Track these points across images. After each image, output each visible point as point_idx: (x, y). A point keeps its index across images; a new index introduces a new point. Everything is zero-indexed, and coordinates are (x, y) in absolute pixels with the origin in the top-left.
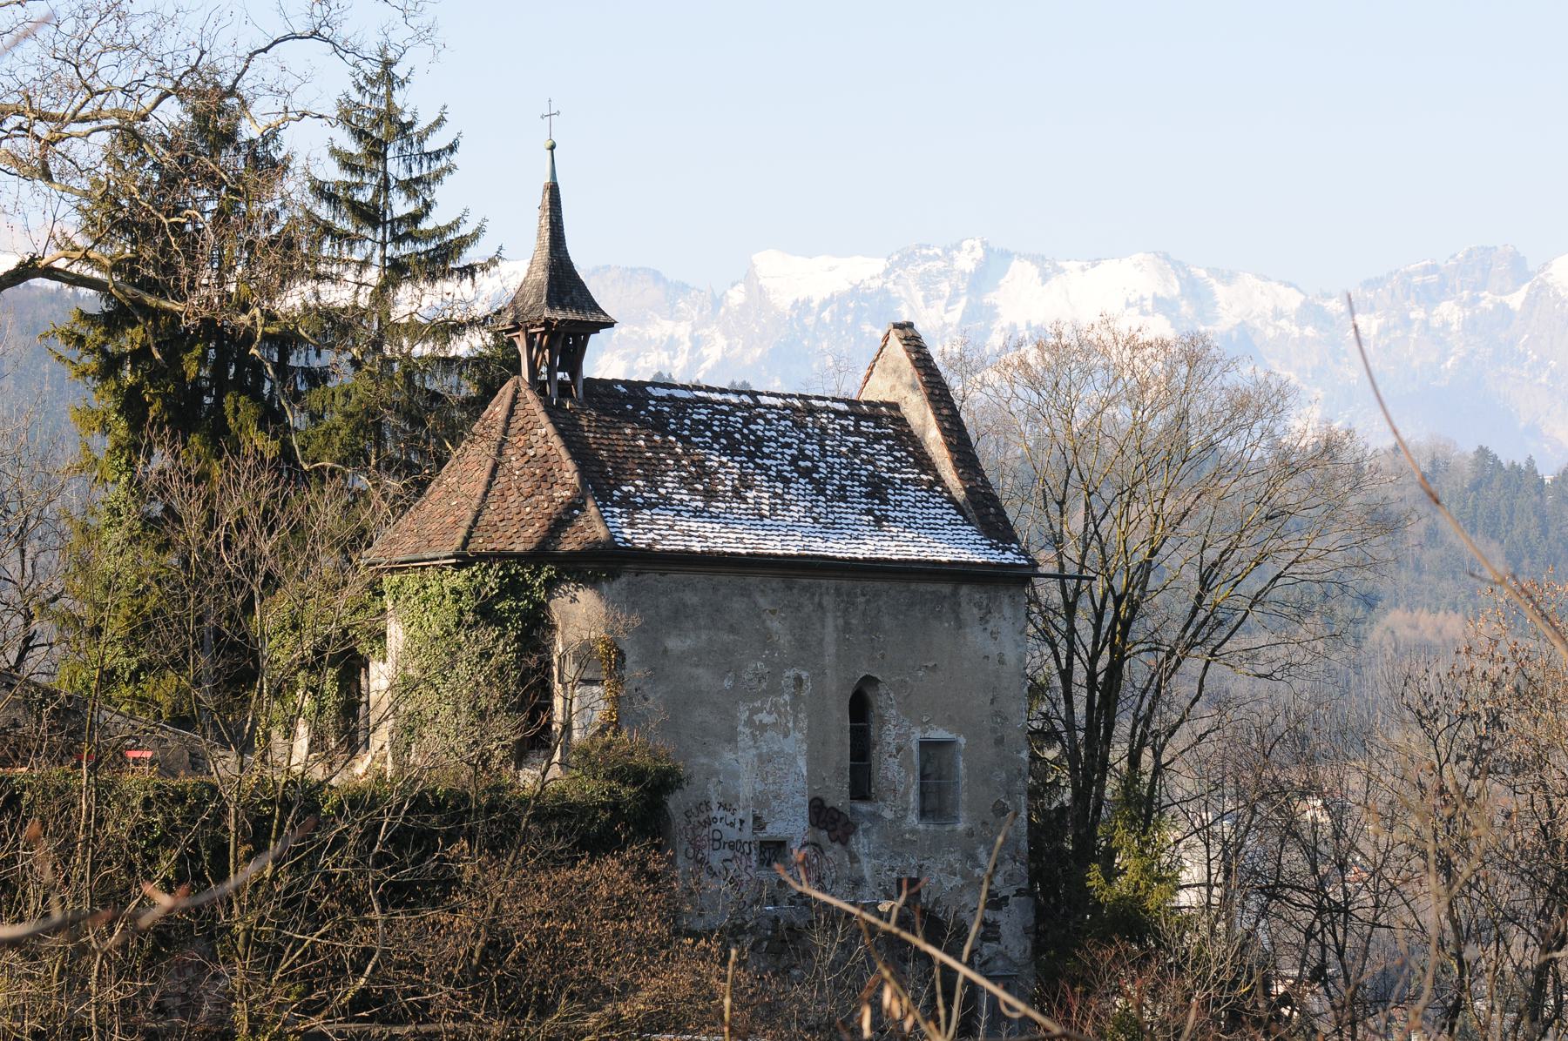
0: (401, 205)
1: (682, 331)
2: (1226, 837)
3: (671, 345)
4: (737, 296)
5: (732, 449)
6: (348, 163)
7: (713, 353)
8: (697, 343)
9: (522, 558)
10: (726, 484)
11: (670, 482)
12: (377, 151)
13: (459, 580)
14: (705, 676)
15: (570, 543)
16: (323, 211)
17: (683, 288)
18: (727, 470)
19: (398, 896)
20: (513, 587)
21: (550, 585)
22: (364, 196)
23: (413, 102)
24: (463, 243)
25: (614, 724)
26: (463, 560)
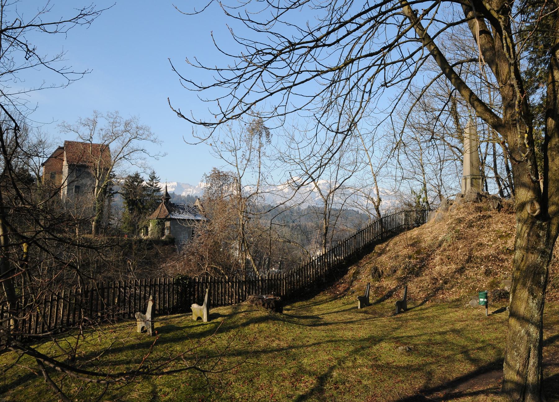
0: (155, 185)
1: (191, 190)
2: (438, 184)
3: (190, 191)
4: (197, 187)
5: (182, 209)
6: (150, 181)
7: (194, 192)
8: (193, 191)
9: (162, 219)
10: (181, 212)
11: (176, 212)
12: (152, 180)
13: (156, 221)
14: (179, 229)
15: (168, 218)
16: (147, 185)
17: (191, 186)
18: (181, 211)
19: (148, 249)
20: (161, 221)
21: (165, 221)
22: (151, 184)
23: (156, 175)
24: (160, 189)
25: (170, 234)
26: (157, 219)
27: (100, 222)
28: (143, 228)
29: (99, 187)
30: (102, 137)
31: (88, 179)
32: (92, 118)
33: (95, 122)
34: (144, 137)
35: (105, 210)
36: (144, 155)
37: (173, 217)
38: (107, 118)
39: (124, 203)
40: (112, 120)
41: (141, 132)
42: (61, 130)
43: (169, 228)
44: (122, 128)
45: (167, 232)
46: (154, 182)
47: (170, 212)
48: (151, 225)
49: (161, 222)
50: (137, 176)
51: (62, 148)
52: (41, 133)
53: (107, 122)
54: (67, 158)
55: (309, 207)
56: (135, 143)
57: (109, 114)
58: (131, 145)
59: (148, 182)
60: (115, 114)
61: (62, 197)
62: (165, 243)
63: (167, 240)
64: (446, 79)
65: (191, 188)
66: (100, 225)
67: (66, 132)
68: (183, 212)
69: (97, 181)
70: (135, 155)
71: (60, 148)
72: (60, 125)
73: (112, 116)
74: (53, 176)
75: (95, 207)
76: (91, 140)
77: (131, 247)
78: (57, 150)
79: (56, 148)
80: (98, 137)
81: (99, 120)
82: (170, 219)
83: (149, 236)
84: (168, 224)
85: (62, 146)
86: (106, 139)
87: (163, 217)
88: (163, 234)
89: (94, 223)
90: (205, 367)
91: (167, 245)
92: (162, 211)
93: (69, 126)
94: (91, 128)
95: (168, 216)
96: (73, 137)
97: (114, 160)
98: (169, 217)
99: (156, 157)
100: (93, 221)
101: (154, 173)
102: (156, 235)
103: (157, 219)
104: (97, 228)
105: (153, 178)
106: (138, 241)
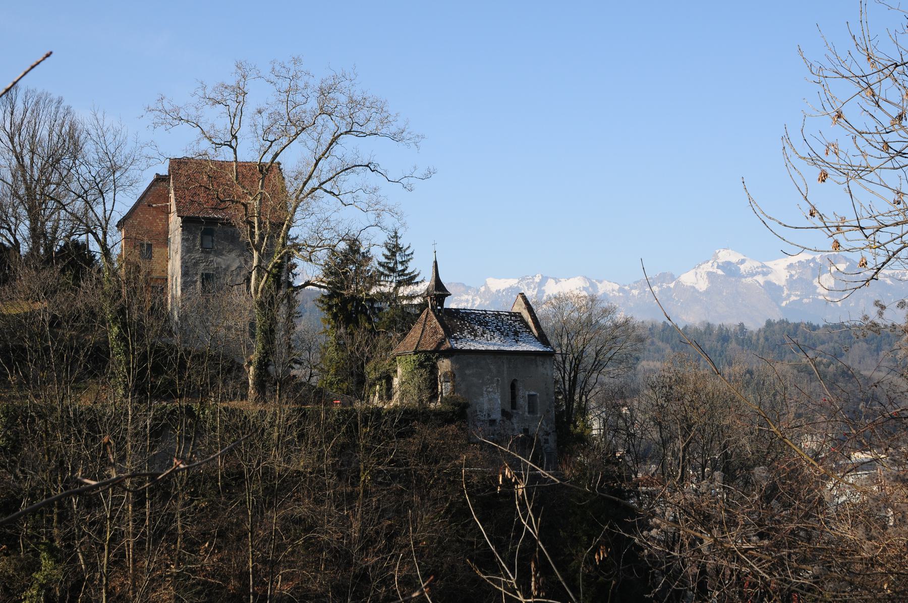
1: (470, 298)
3: (467, 301)
4: (483, 289)
5: (480, 325)
6: (387, 257)
7: (477, 303)
8: (473, 300)
9: (430, 352)
12: (394, 254)
13: (415, 357)
16: (381, 269)
17: (470, 287)
18: (479, 329)
19: (400, 435)
21: (437, 358)
22: (391, 265)
23: (402, 242)
24: (415, 276)
26: (416, 353)
27: (267, 365)
28: (380, 379)
30: (260, 132)
31: (233, 255)
32: (232, 82)
33: (240, 93)
34: (371, 127)
35: (280, 335)
37: (459, 346)
38: (273, 78)
39: (324, 320)
40: (285, 85)
41: (360, 116)
42: (156, 120)
43: (451, 377)
44: (313, 104)
45: (445, 388)
46: (399, 258)
47: (449, 333)
48: (400, 371)
50: (354, 245)
52: (105, 129)
53: (273, 89)
54: (178, 203)
55: (769, 324)
56: (348, 147)
57: (277, 68)
58: (337, 149)
59: (383, 260)
60: (291, 66)
61: (169, 307)
62: (444, 418)
63: (448, 408)
64: (395, 394)
65: (468, 294)
67: (168, 126)
68: (484, 332)
69: (256, 254)
70: (349, 181)
71: (159, 179)
72: (152, 107)
73: (284, 72)
74: (147, 252)
75: (252, 325)
76: (234, 144)
77: (352, 431)
80: (251, 135)
81: (251, 86)
82: (451, 353)
83: (395, 400)
84: (445, 365)
85: (164, 171)
88: (434, 397)
89: (252, 368)
91: (450, 421)
93: (177, 110)
94: (233, 110)
97: (297, 197)
98: (448, 345)
99: (404, 181)
100: (250, 363)
101: (396, 237)
102: (413, 400)
103: (416, 353)
104: (261, 385)
105: (394, 249)
106: (372, 413)
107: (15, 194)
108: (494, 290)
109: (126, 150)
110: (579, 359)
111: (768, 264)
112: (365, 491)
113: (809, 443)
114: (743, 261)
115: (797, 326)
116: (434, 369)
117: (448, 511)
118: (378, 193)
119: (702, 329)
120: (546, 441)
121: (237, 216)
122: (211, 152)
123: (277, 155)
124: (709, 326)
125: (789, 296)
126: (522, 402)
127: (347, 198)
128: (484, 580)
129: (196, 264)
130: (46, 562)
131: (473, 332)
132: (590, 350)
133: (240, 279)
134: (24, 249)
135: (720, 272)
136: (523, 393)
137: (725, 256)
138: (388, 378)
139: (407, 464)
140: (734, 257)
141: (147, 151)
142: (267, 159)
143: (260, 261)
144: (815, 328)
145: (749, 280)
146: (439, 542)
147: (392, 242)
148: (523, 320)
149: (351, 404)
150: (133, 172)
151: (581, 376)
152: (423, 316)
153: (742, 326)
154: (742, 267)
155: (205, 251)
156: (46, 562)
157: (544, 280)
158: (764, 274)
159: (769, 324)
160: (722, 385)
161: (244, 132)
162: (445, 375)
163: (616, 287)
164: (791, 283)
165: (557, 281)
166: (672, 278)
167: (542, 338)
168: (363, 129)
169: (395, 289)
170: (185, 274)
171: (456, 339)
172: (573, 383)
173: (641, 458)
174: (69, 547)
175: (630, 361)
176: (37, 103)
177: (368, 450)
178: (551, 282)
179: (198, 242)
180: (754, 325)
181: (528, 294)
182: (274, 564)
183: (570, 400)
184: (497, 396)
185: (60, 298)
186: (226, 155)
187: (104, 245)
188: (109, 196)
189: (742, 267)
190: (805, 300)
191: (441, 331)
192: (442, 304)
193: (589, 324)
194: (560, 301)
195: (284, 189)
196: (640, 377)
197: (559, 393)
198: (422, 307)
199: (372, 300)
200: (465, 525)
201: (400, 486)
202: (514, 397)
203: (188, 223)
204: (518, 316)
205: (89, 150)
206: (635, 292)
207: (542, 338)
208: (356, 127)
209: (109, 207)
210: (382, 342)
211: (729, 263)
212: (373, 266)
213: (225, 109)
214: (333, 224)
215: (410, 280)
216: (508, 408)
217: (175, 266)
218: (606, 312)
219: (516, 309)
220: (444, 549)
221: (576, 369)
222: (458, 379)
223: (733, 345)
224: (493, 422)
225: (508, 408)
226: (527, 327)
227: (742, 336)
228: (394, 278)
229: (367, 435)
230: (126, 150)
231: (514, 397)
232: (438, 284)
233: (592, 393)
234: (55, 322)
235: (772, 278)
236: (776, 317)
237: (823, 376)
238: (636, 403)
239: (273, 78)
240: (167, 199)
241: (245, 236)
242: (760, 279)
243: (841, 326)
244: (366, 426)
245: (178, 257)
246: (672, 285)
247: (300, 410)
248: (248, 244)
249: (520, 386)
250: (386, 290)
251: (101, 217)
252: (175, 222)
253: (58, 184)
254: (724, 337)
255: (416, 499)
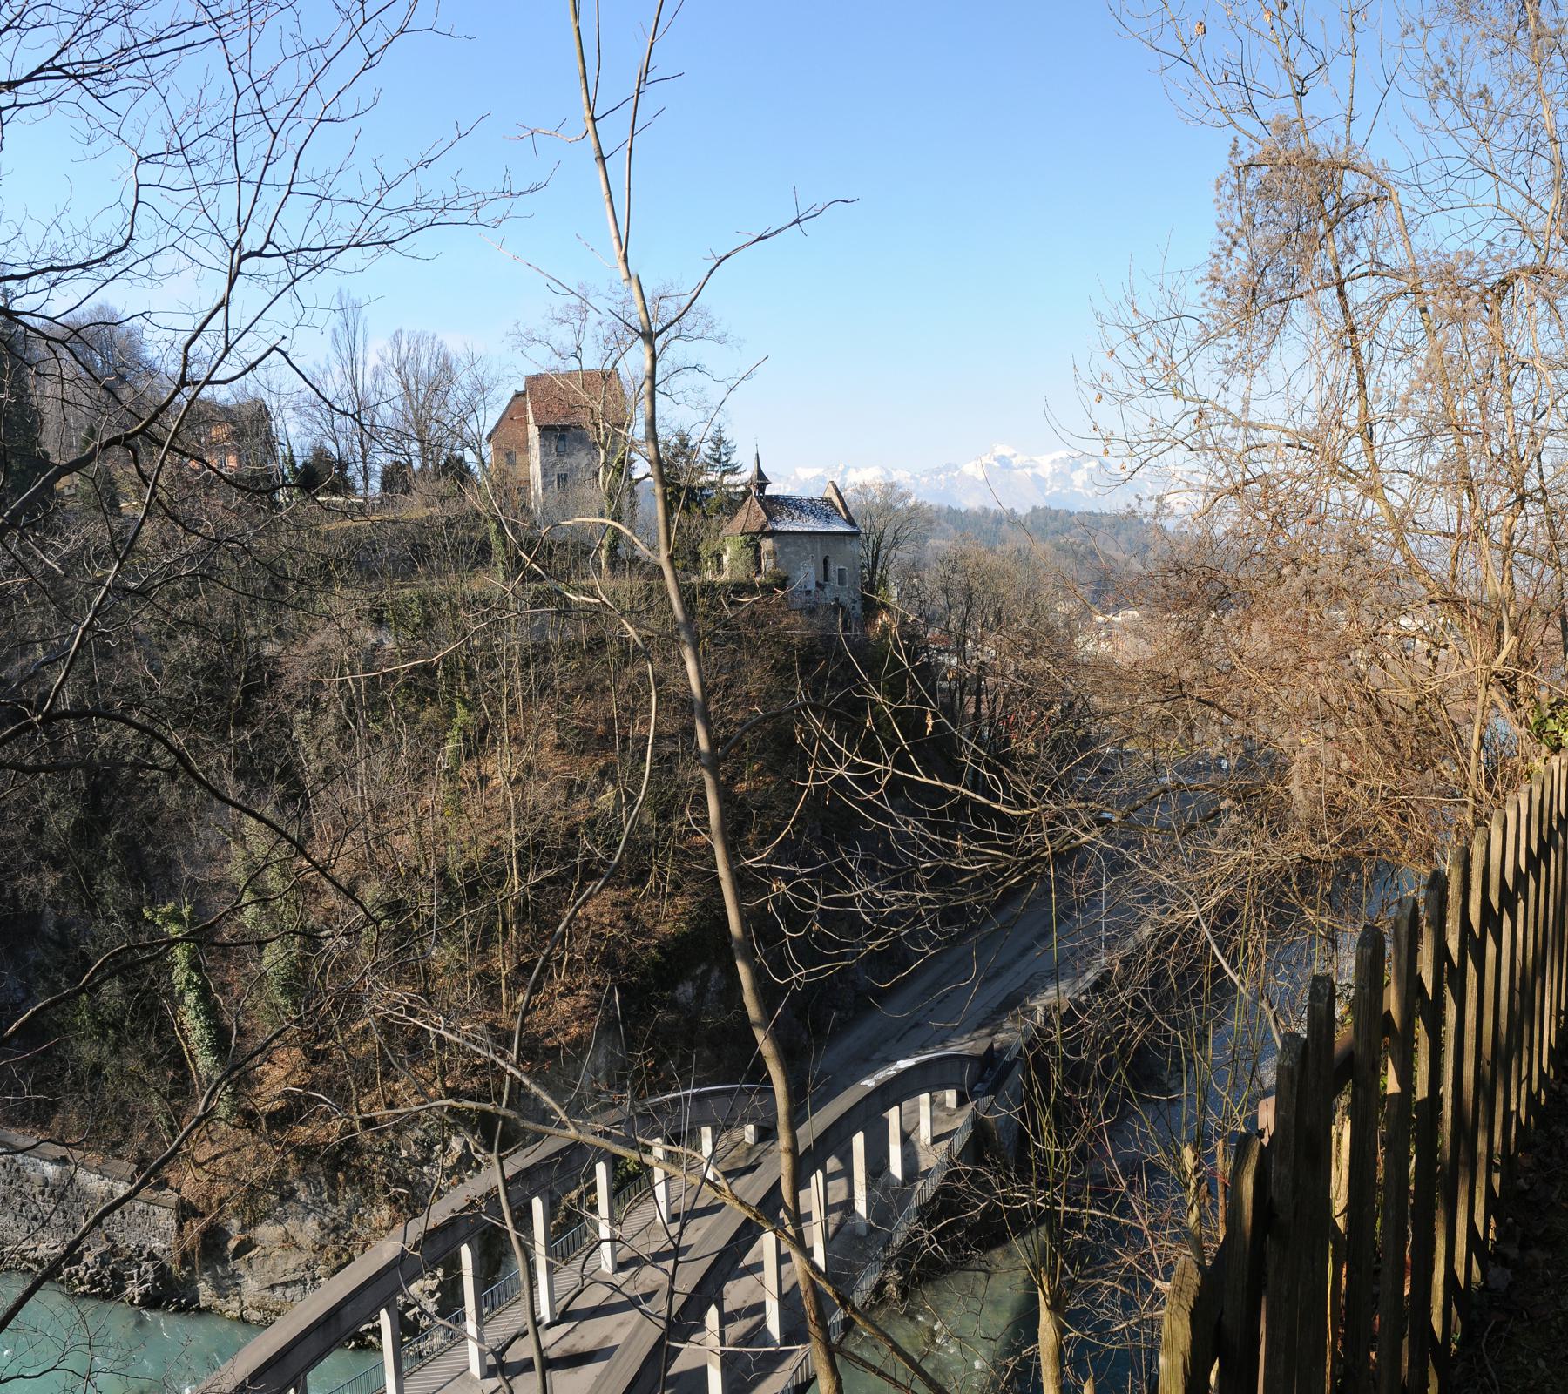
17: (781, 476)
18: (796, 513)
27: (616, 548)
29: (606, 464)
31: (582, 454)
34: (697, 331)
36: (698, 379)
37: (778, 528)
38: (610, 295)
45: (767, 564)
46: (723, 450)
47: (770, 516)
48: (728, 550)
49: (752, 542)
51: (523, 394)
54: (535, 414)
55: (1035, 509)
57: (614, 285)
59: (709, 452)
66: (617, 555)
69: (602, 452)
71: (518, 395)
78: (512, 400)
79: (511, 394)
82: (773, 534)
83: (725, 577)
84: (767, 544)
85: (521, 388)
86: (611, 347)
87: (756, 529)
88: (759, 572)
90: (450, 741)
92: (750, 516)
94: (577, 327)
95: (764, 526)
96: (540, 361)
98: (769, 527)
101: (720, 431)
107: (407, 420)
108: (802, 478)
109: (492, 373)
110: (880, 539)
111: (1035, 458)
112: (704, 652)
113: (1062, 608)
114: (1015, 456)
115: (1057, 512)
116: (758, 548)
117: (773, 666)
118: (705, 392)
119: (980, 512)
120: (854, 608)
121: (586, 420)
122: (561, 366)
123: (616, 362)
124: (986, 510)
125: (1052, 487)
126: (833, 575)
127: (679, 398)
128: (944, 716)
129: (553, 466)
130: (461, 711)
131: (791, 516)
132: (889, 532)
133: (590, 475)
134: (417, 464)
135: (996, 464)
136: (834, 568)
137: (1001, 450)
138: (718, 557)
139: (738, 628)
140: (1008, 452)
141: (508, 371)
142: (608, 366)
143: (606, 458)
144: (1071, 515)
145: (1019, 471)
146: (767, 693)
147: (717, 436)
148: (833, 505)
149: (688, 578)
150: (497, 392)
151: (882, 553)
152: (748, 502)
153: (1012, 510)
154: (1014, 460)
155: (559, 454)
156: (461, 711)
157: (846, 469)
158: (1032, 467)
159: (1035, 509)
160: (998, 562)
161: (587, 342)
162: (768, 553)
163: (909, 475)
164: (1054, 476)
165: (858, 470)
166: (956, 468)
167: (850, 521)
168: (690, 334)
169: (721, 478)
170: (544, 475)
171: (777, 522)
172: (876, 557)
173: (929, 622)
174: (476, 699)
175: (920, 540)
176: (417, 342)
177: (706, 617)
178: (852, 471)
179: (553, 448)
180: (1023, 510)
181: (837, 482)
182: (634, 712)
183: (872, 574)
184: (812, 570)
185: (451, 503)
186: (573, 365)
187: (479, 455)
188: (481, 413)
189: (1014, 460)
190: (1064, 491)
191: (763, 514)
192: (763, 492)
193: (886, 508)
194: (863, 490)
195: (623, 394)
196: (929, 554)
197: (863, 567)
198: (746, 495)
199: (702, 489)
200: (789, 678)
201: (733, 646)
202: (826, 570)
203: (545, 431)
204: (829, 501)
205: (464, 378)
206: (925, 479)
207: (850, 521)
208: (684, 332)
209: (481, 423)
210: (714, 525)
211: (1004, 456)
212: (700, 458)
213: (571, 327)
214: (668, 422)
215: (734, 471)
216: (821, 581)
217: (535, 469)
218: (904, 496)
219: (827, 495)
220: (771, 697)
221: (878, 546)
222: (779, 556)
223: (1005, 527)
224: (808, 592)
225: (821, 581)
226: (837, 510)
227: (1012, 519)
228: (719, 468)
229: (704, 604)
230: (492, 373)
231: (826, 570)
232: (760, 475)
233: (892, 566)
234: (450, 524)
235: (1039, 471)
236: (1041, 504)
237: (1075, 553)
238: (926, 576)
239: (610, 295)
240: (525, 411)
241: (592, 438)
242: (1028, 471)
243: (1091, 514)
244: (703, 596)
245: (538, 461)
246: (956, 474)
247: (646, 585)
248: (595, 443)
249: (831, 561)
250: (712, 479)
251: (476, 431)
252: (533, 432)
253: (439, 408)
254: (998, 520)
255: (747, 657)
